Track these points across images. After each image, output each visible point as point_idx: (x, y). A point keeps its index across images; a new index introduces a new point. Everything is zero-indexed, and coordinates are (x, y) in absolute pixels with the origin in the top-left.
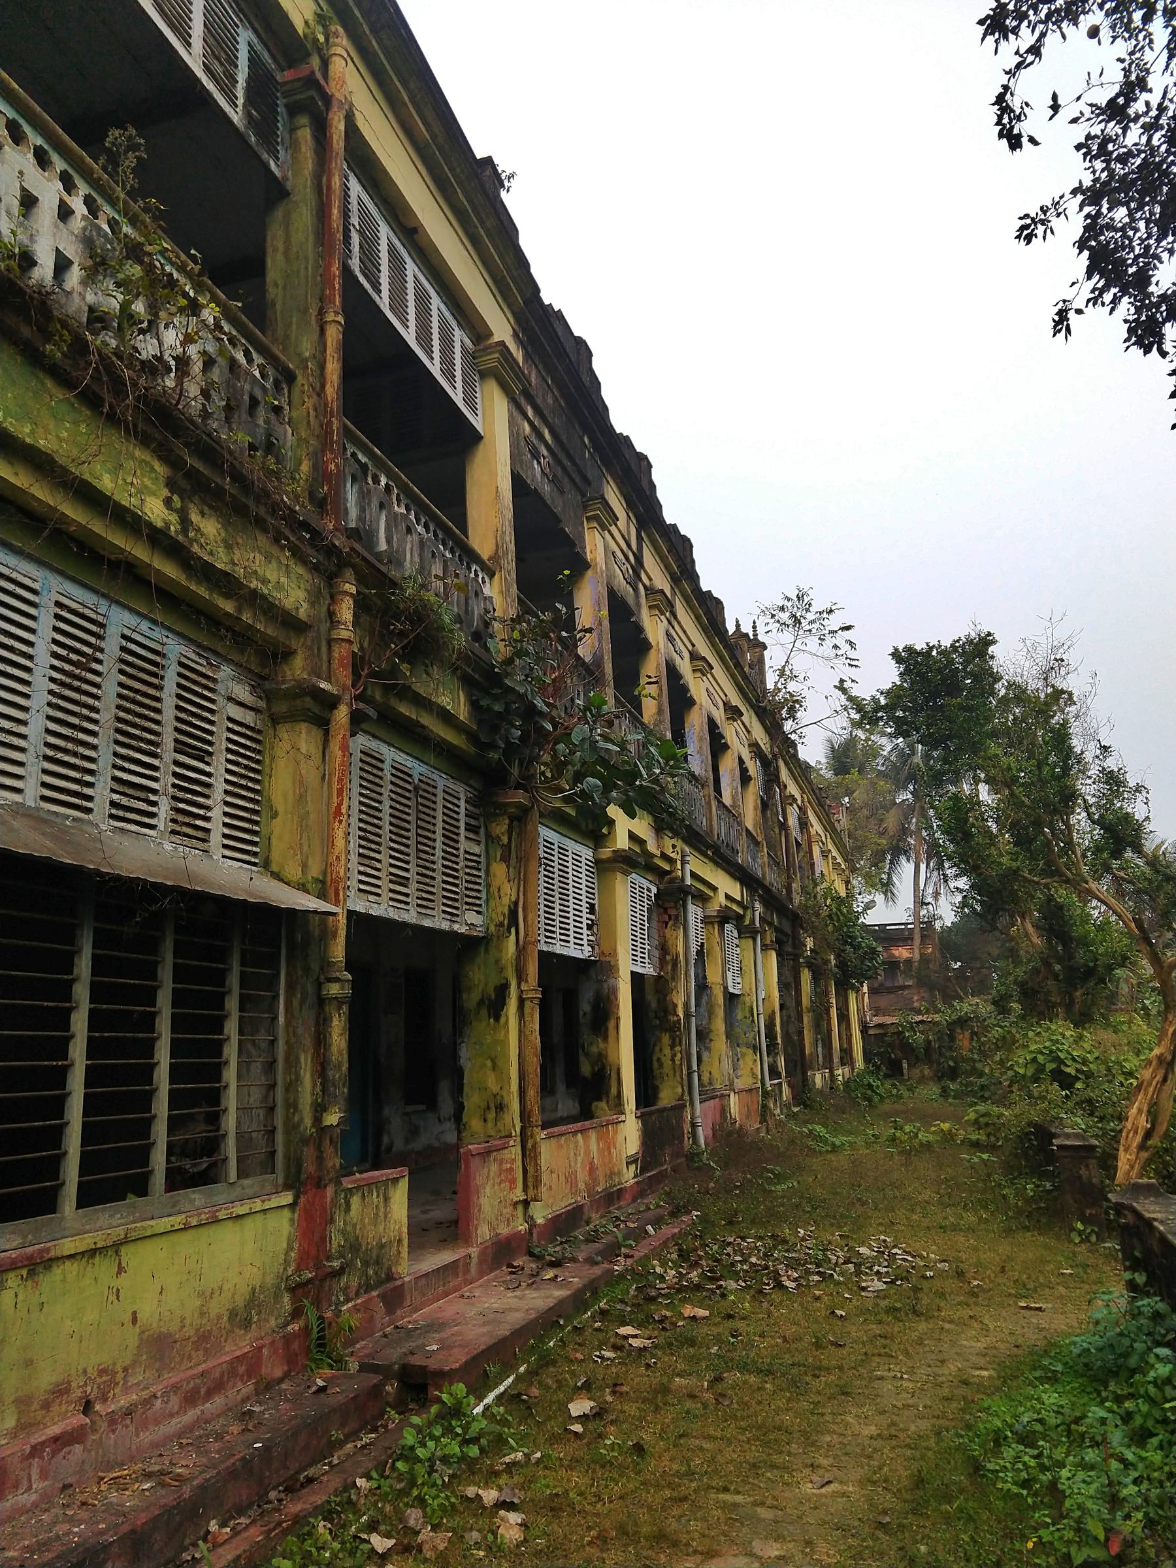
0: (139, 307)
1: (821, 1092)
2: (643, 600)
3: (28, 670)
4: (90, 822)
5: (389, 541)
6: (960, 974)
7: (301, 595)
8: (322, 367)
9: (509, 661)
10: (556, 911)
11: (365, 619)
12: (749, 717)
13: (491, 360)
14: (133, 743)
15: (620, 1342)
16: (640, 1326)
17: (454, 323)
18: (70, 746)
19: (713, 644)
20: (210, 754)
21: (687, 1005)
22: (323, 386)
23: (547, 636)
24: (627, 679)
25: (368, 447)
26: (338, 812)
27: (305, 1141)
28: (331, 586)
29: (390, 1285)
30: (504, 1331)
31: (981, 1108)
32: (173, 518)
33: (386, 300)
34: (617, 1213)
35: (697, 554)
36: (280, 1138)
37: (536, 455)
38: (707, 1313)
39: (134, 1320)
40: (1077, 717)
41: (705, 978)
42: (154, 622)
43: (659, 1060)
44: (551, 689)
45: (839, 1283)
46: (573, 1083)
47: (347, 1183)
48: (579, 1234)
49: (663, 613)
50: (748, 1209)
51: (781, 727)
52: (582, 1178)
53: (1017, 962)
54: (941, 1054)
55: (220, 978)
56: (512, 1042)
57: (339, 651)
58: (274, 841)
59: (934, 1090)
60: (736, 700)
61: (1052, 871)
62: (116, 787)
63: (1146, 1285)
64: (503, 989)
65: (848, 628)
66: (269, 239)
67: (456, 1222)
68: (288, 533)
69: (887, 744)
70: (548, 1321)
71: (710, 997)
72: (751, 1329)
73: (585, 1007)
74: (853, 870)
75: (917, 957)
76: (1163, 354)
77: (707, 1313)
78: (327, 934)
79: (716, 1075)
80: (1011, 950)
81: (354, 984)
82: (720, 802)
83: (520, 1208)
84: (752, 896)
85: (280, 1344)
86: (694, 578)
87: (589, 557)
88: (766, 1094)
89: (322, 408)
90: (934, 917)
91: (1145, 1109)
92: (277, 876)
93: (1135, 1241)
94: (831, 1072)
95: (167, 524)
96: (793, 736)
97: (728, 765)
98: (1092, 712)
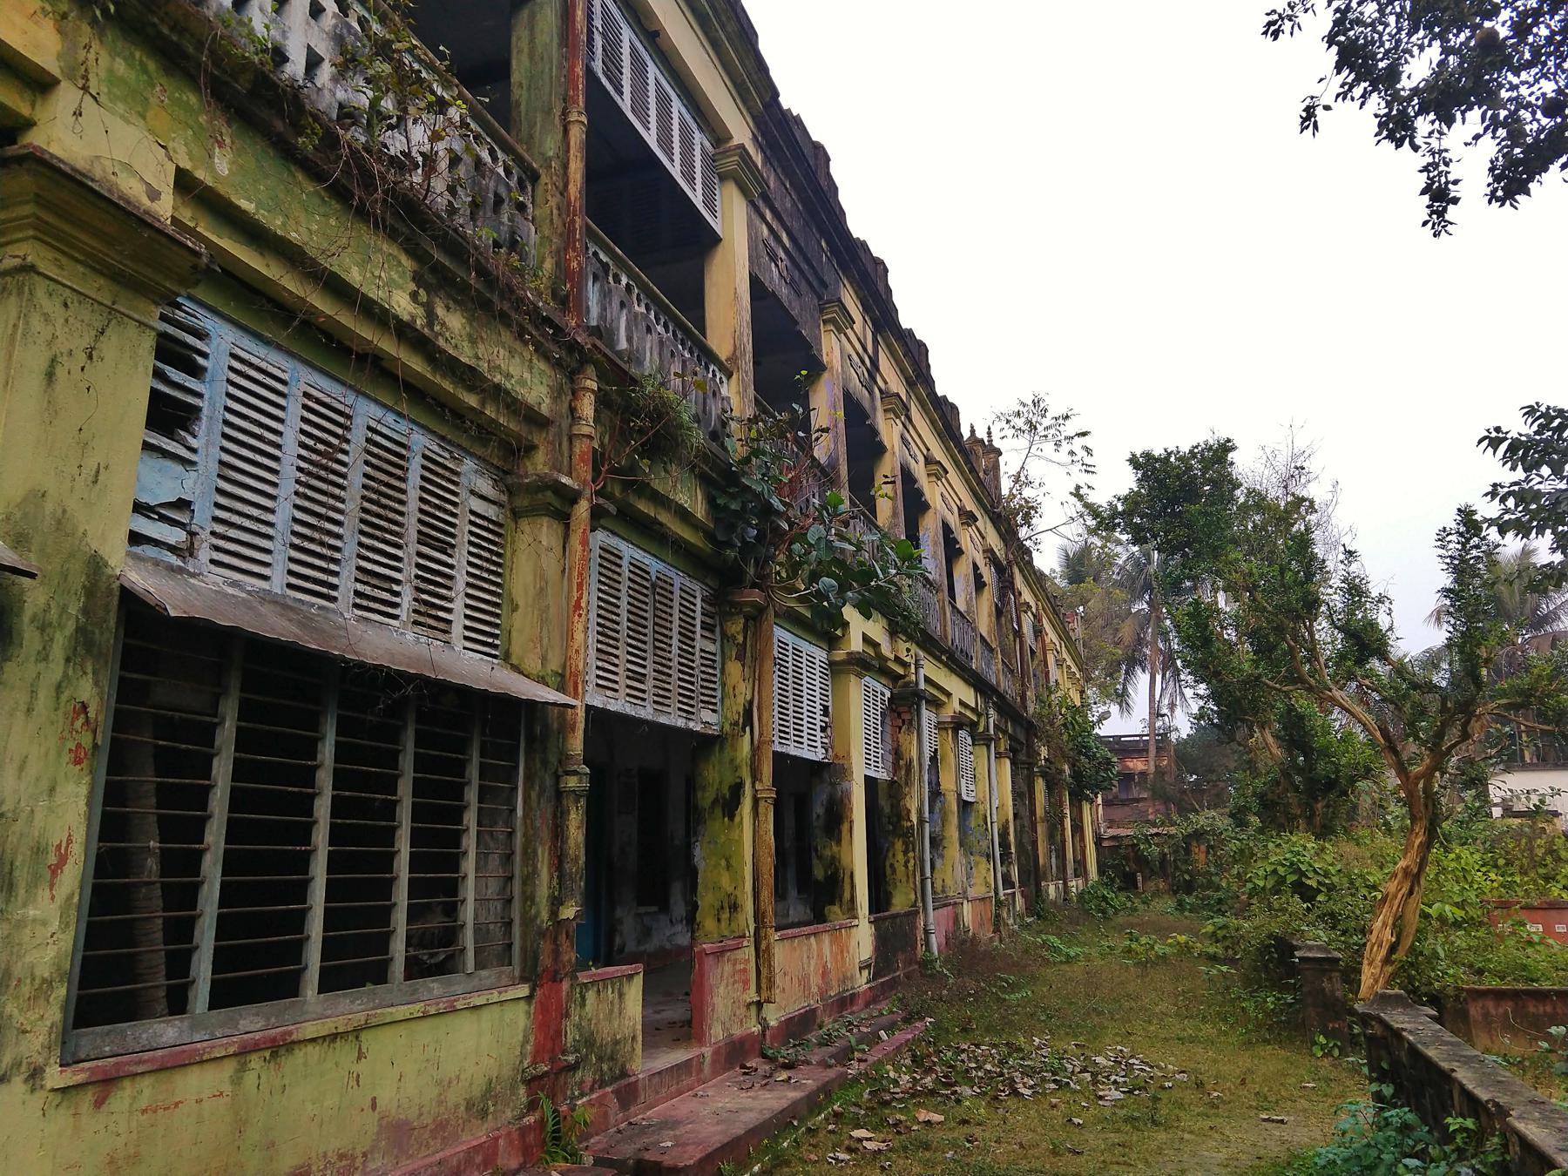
0: (388, 104)
1: (1054, 903)
2: (878, 403)
3: (276, 459)
4: (334, 611)
5: (629, 339)
6: (1197, 788)
7: (544, 390)
8: (565, 166)
9: (746, 461)
10: (790, 712)
11: (606, 414)
12: (984, 523)
13: (731, 163)
14: (378, 533)
15: (854, 1145)
16: (874, 1129)
17: (694, 126)
18: (316, 535)
19: (948, 449)
20: (453, 546)
21: (920, 812)
22: (566, 185)
23: (782, 436)
24: (862, 485)
25: (608, 245)
26: (578, 606)
27: (542, 934)
28: (572, 381)
29: (624, 1082)
30: (739, 1130)
31: (1220, 920)
32: (420, 311)
33: (628, 102)
34: (850, 1018)
35: (933, 359)
36: (517, 930)
37: (773, 258)
38: (942, 1118)
39: (374, 1106)
40: (1318, 524)
41: (938, 784)
42: (400, 414)
43: (892, 865)
44: (786, 489)
45: (1075, 1091)
46: (807, 887)
47: (583, 978)
48: (812, 1037)
49: (898, 417)
50: (982, 1017)
51: (1016, 533)
52: (815, 981)
53: (1255, 773)
54: (1177, 868)
55: (460, 768)
56: (745, 843)
57: (581, 447)
58: (514, 634)
59: (1168, 904)
60: (970, 505)
61: (1295, 679)
62: (361, 577)
63: (1393, 1096)
64: (737, 789)
65: (1084, 434)
66: (514, 39)
67: (689, 1023)
68: (530, 327)
69: (1124, 549)
70: (782, 1122)
71: (943, 803)
72: (987, 1135)
73: (819, 810)
74: (1088, 679)
75: (1152, 769)
76: (1416, 148)
77: (942, 1118)
78: (565, 728)
79: (949, 882)
80: (1250, 762)
81: (593, 778)
82: (954, 607)
83: (753, 1009)
84: (986, 703)
85: (515, 1136)
86: (929, 382)
87: (825, 359)
88: (999, 904)
89: (565, 208)
90: (1169, 729)
91: (1390, 922)
92: (517, 669)
93: (1383, 1053)
94: (1065, 884)
95: (414, 318)
96: (1027, 543)
97: (962, 571)
98: (1333, 521)
